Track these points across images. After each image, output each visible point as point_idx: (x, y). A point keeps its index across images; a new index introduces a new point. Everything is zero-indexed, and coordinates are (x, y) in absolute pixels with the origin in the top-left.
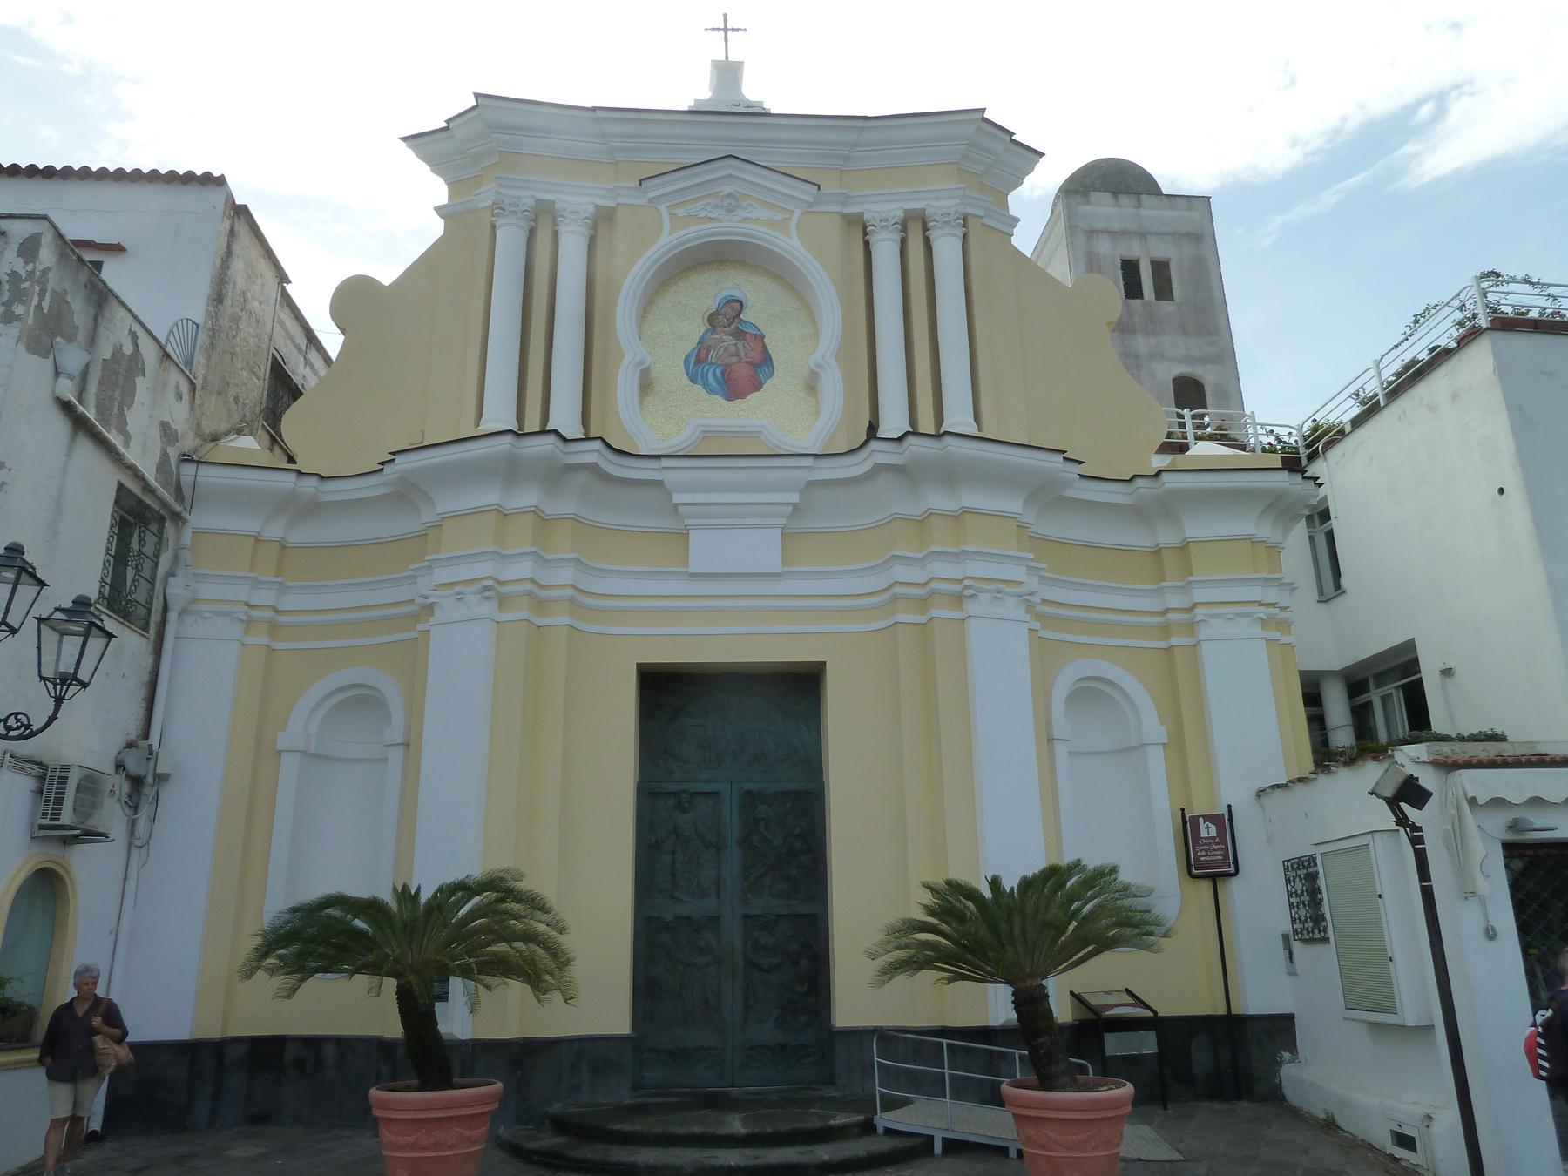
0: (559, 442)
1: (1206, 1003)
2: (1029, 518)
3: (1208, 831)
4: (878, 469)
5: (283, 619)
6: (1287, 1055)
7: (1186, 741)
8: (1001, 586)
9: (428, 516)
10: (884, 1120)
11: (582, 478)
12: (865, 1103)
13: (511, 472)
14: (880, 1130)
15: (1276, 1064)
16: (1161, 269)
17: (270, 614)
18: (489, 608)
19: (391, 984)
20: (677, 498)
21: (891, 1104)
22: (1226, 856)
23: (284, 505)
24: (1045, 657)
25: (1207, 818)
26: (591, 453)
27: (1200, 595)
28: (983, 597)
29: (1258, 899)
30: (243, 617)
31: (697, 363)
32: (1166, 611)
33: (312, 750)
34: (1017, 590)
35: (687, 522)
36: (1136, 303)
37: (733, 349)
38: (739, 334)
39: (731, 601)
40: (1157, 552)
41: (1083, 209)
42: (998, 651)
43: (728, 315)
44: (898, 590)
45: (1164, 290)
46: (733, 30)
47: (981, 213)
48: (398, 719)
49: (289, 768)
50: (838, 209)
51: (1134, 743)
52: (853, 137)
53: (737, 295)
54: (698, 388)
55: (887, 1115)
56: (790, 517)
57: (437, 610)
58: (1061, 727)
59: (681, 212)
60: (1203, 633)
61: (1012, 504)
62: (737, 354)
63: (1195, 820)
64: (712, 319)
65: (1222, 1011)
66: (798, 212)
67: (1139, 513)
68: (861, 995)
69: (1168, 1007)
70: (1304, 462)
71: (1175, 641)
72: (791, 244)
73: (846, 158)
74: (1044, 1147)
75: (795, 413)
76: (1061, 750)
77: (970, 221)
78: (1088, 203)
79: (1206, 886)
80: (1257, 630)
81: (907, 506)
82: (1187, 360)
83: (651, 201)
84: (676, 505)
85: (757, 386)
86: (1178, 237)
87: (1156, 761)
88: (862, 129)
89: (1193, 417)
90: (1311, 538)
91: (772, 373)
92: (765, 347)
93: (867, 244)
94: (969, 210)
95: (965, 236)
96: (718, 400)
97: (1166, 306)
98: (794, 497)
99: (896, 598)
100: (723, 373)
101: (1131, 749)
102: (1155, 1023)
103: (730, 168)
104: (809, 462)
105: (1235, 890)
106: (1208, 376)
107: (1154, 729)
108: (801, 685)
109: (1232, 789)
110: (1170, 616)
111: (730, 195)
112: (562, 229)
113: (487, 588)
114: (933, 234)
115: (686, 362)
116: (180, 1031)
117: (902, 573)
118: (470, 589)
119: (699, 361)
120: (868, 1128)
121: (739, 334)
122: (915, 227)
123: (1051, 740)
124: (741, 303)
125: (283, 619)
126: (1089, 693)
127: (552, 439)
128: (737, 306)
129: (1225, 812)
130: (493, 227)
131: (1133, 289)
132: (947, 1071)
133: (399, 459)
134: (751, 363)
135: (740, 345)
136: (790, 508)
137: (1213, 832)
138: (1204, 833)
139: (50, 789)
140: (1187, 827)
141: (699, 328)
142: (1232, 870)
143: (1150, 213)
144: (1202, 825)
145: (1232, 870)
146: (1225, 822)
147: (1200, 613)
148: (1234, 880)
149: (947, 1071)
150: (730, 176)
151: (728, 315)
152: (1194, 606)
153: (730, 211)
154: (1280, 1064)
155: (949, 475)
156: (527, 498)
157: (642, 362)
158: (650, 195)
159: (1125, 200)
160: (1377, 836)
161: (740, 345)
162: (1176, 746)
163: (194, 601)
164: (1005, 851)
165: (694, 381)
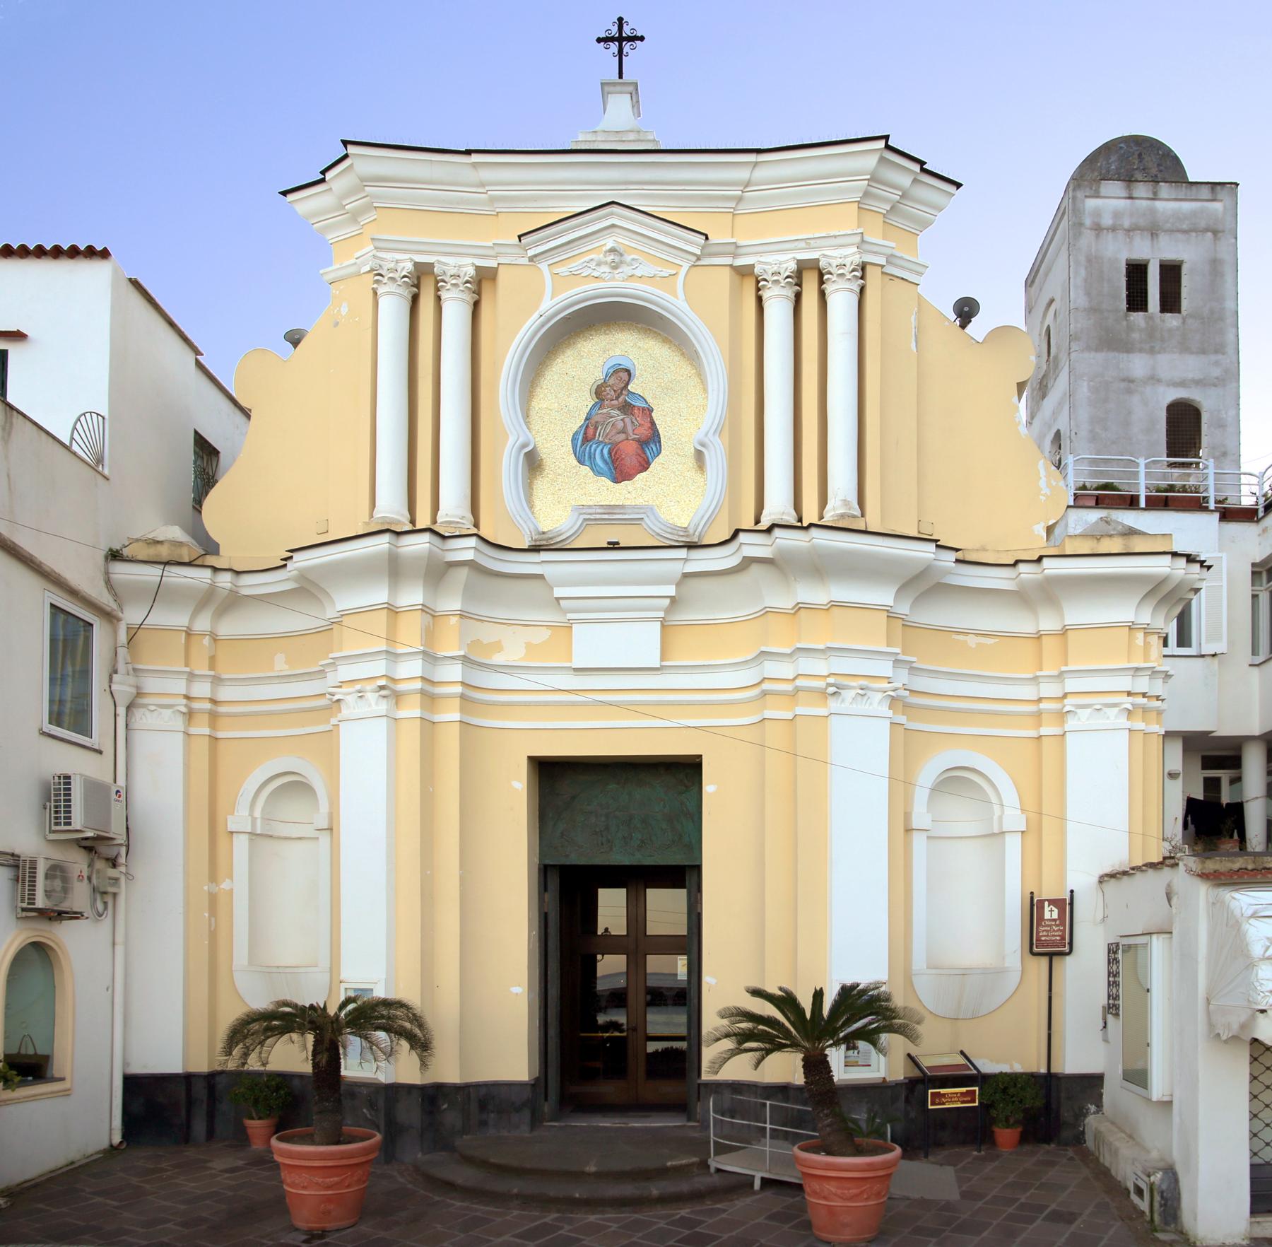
0: (436, 540)
1: (1027, 1060)
2: (904, 609)
3: (1050, 913)
4: (748, 562)
5: (222, 709)
6: (1093, 1108)
7: (1045, 821)
8: (864, 682)
9: (330, 613)
10: (714, 1163)
11: (464, 573)
12: (701, 1146)
13: (394, 569)
14: (712, 1170)
15: (1081, 1114)
16: (1171, 273)
17: (208, 706)
18: (383, 707)
19: (310, 1038)
20: (558, 592)
21: (721, 1150)
22: (1063, 938)
23: (205, 599)
24: (905, 748)
25: (1051, 902)
26: (466, 550)
27: (1071, 684)
28: (849, 695)
29: (1084, 972)
30: (184, 710)
31: (585, 440)
32: (1040, 700)
33: (259, 832)
34: (885, 685)
35: (570, 616)
36: (1137, 317)
37: (620, 425)
38: (627, 408)
39: (604, 676)
40: (1039, 637)
41: (1091, 203)
42: (858, 745)
43: (615, 389)
44: (766, 686)
45: (1170, 302)
46: (612, 39)
47: (883, 261)
48: (324, 808)
49: (241, 845)
50: (728, 261)
51: (996, 831)
52: (743, 174)
53: (627, 365)
54: (585, 470)
55: (718, 1158)
56: (668, 611)
57: (343, 705)
58: (921, 816)
59: (562, 270)
60: (1071, 723)
61: (884, 596)
62: (624, 431)
63: (1041, 902)
64: (599, 392)
65: (1043, 1070)
66: (686, 266)
67: (1022, 598)
68: (723, 1063)
69: (988, 1066)
70: (1261, 514)
71: (1044, 731)
72: (674, 301)
73: (739, 200)
74: (825, 1198)
75: (674, 493)
76: (919, 841)
77: (868, 268)
78: (1097, 195)
79: (1044, 961)
80: (1123, 721)
81: (781, 599)
82: (1182, 384)
83: (531, 259)
84: (558, 599)
85: (645, 466)
86: (1190, 229)
87: (1013, 846)
88: (756, 164)
89: (1147, 466)
90: (1255, 597)
91: (659, 453)
92: (653, 423)
93: (759, 300)
94: (868, 258)
95: (862, 289)
96: (605, 482)
97: (1171, 320)
98: (671, 590)
99: (765, 693)
100: (610, 453)
101: (993, 835)
102: (982, 1079)
103: (615, 209)
104: (682, 553)
105: (1069, 968)
106: (1207, 402)
107: (1014, 819)
108: (687, 770)
109: (1080, 877)
110: (1043, 706)
111: (612, 250)
112: (444, 295)
113: (382, 688)
114: (828, 288)
115: (574, 440)
116: (174, 1066)
117: (772, 668)
118: (369, 687)
119: (586, 439)
120: (704, 1165)
121: (627, 408)
122: (808, 274)
123: (908, 830)
124: (628, 371)
125: (222, 709)
126: (955, 782)
127: (426, 537)
128: (624, 376)
129: (1068, 897)
130: (375, 293)
131: (1137, 300)
132: (768, 1126)
133: (297, 556)
134: (638, 441)
135: (627, 420)
136: (667, 601)
137: (1055, 915)
138: (1047, 915)
139: (24, 874)
140: (1034, 908)
141: (585, 402)
142: (1067, 949)
143: (1169, 205)
144: (1047, 909)
145: (1067, 949)
146: (1066, 905)
147: (1069, 703)
148: (1068, 958)
149: (768, 1126)
150: (613, 226)
151: (615, 389)
152: (1065, 695)
153: (615, 268)
154: (1085, 1115)
155: (819, 568)
156: (412, 596)
157: (524, 446)
158: (531, 253)
159: (1142, 190)
160: (1154, 937)
161: (627, 420)
162: (1032, 833)
163: (139, 694)
164: (850, 957)
165: (581, 462)
